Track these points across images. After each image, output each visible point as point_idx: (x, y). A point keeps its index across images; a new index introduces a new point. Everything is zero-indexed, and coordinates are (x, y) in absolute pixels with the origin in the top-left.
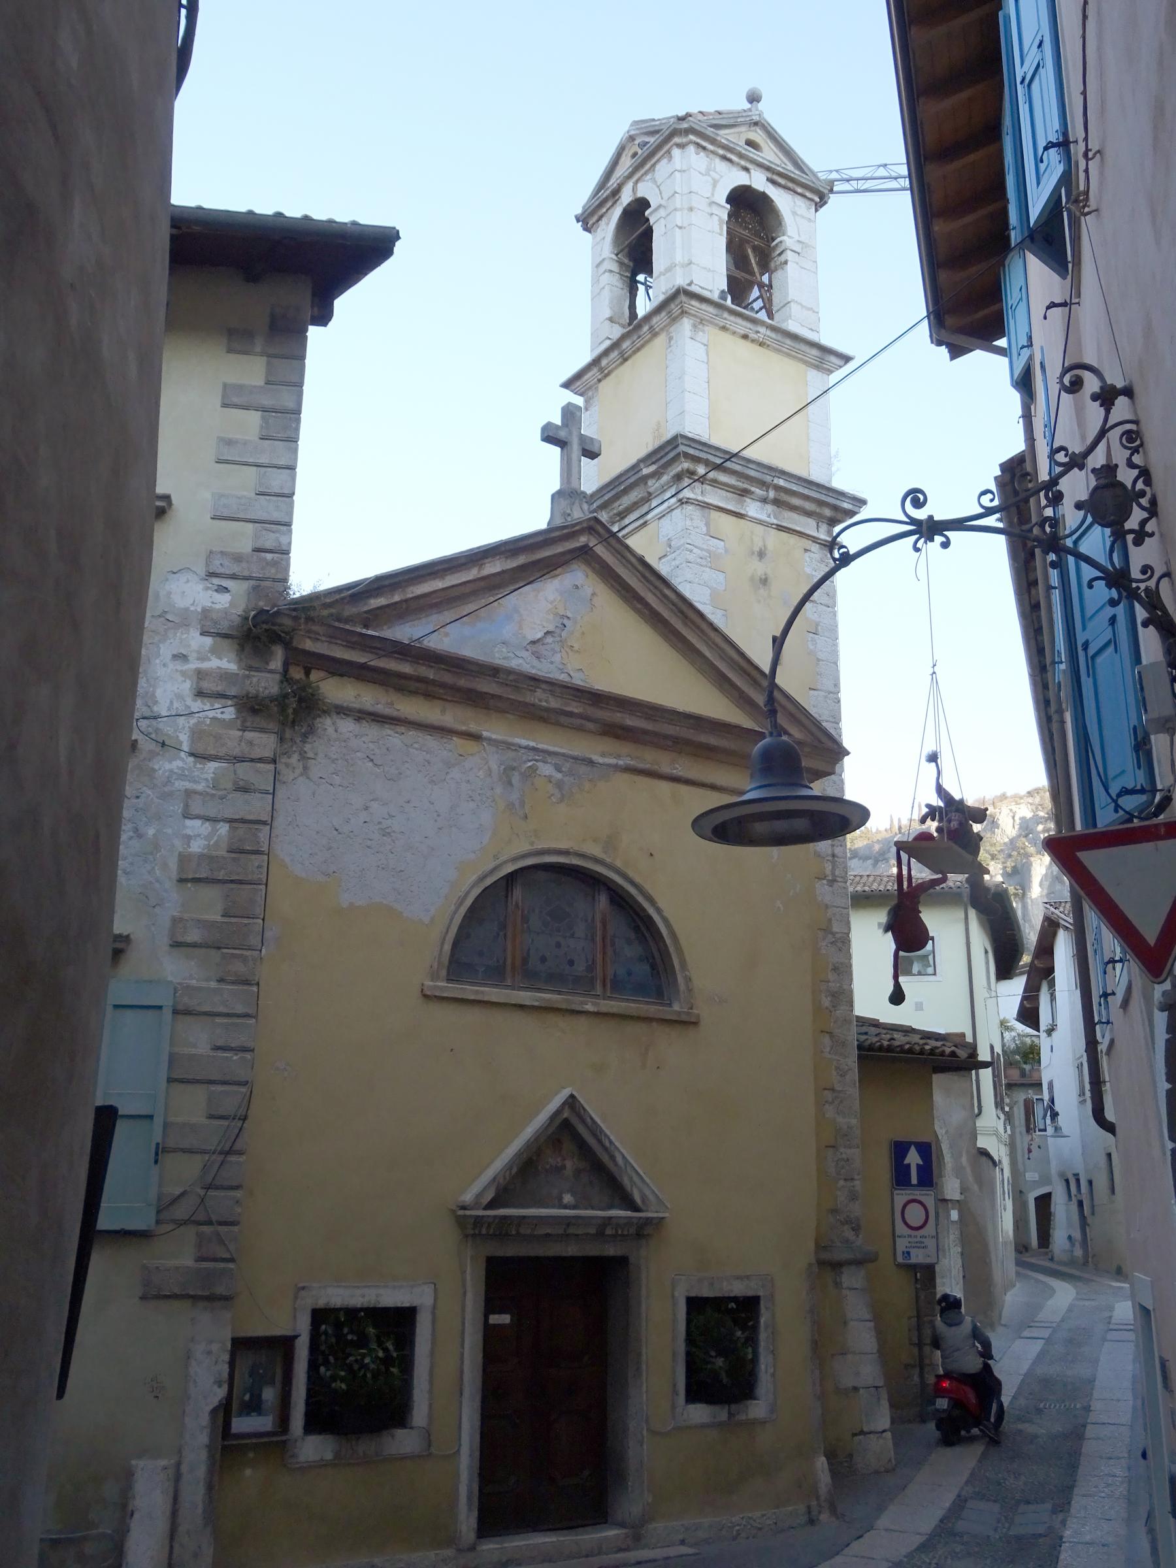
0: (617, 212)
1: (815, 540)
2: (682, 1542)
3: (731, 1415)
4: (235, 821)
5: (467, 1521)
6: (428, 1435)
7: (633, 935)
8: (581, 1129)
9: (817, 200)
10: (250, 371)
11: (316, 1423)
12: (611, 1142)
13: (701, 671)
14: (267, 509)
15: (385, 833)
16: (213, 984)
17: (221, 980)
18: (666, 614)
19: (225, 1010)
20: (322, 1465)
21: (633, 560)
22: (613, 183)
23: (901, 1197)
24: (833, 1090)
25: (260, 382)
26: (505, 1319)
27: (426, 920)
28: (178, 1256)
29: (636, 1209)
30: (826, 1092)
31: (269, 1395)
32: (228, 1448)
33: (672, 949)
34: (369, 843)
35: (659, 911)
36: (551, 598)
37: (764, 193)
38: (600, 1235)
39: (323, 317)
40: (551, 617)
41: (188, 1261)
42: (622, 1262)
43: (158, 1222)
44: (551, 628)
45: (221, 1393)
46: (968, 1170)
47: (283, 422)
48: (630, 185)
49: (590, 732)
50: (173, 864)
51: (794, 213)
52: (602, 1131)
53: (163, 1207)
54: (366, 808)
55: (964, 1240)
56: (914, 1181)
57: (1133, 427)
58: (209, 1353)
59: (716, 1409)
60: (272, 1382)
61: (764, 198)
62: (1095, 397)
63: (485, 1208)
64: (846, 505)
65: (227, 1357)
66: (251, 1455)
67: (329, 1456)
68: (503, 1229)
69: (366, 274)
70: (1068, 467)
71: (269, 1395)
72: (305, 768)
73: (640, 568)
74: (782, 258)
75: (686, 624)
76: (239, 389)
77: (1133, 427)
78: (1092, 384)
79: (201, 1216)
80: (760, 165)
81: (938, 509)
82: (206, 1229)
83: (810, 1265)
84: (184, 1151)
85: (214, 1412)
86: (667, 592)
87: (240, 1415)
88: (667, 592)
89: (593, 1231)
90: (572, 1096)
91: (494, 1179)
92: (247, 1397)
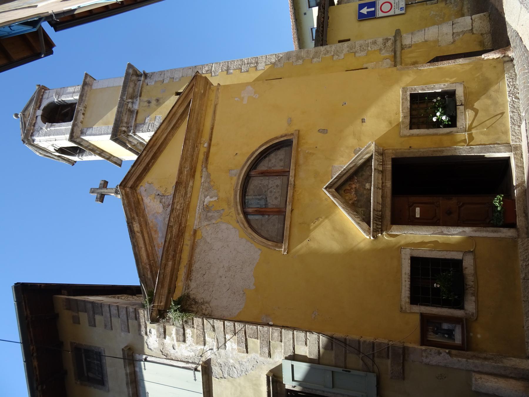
1: (144, 81)
2: (519, 126)
3: (462, 105)
4: (224, 332)
5: (506, 233)
7: (267, 159)
11: (459, 304)
12: (344, 170)
13: (173, 136)
15: (229, 269)
16: (283, 344)
17: (281, 341)
18: (152, 154)
20: (477, 302)
21: (133, 169)
23: (379, 14)
24: (333, 56)
27: (260, 252)
28: (387, 365)
29: (372, 155)
30: (334, 59)
31: (445, 326)
32: (467, 346)
33: (271, 144)
34: (232, 277)
35: (257, 150)
36: (149, 200)
37: (43, 110)
38: (382, 172)
40: (155, 200)
41: (389, 362)
43: (374, 372)
44: (159, 200)
50: (243, 355)
51: (48, 98)
52: (340, 174)
53: (368, 370)
54: (221, 277)
56: (373, 9)
58: (427, 357)
64: (131, 71)
66: (471, 334)
67: (473, 298)
68: (380, 218)
71: (445, 326)
72: (207, 303)
73: (135, 167)
75: (156, 145)
76: (90, 322)
79: (371, 357)
80: (35, 113)
82: (376, 355)
84: (345, 360)
87: (454, 340)
90: (326, 188)
92: (446, 336)
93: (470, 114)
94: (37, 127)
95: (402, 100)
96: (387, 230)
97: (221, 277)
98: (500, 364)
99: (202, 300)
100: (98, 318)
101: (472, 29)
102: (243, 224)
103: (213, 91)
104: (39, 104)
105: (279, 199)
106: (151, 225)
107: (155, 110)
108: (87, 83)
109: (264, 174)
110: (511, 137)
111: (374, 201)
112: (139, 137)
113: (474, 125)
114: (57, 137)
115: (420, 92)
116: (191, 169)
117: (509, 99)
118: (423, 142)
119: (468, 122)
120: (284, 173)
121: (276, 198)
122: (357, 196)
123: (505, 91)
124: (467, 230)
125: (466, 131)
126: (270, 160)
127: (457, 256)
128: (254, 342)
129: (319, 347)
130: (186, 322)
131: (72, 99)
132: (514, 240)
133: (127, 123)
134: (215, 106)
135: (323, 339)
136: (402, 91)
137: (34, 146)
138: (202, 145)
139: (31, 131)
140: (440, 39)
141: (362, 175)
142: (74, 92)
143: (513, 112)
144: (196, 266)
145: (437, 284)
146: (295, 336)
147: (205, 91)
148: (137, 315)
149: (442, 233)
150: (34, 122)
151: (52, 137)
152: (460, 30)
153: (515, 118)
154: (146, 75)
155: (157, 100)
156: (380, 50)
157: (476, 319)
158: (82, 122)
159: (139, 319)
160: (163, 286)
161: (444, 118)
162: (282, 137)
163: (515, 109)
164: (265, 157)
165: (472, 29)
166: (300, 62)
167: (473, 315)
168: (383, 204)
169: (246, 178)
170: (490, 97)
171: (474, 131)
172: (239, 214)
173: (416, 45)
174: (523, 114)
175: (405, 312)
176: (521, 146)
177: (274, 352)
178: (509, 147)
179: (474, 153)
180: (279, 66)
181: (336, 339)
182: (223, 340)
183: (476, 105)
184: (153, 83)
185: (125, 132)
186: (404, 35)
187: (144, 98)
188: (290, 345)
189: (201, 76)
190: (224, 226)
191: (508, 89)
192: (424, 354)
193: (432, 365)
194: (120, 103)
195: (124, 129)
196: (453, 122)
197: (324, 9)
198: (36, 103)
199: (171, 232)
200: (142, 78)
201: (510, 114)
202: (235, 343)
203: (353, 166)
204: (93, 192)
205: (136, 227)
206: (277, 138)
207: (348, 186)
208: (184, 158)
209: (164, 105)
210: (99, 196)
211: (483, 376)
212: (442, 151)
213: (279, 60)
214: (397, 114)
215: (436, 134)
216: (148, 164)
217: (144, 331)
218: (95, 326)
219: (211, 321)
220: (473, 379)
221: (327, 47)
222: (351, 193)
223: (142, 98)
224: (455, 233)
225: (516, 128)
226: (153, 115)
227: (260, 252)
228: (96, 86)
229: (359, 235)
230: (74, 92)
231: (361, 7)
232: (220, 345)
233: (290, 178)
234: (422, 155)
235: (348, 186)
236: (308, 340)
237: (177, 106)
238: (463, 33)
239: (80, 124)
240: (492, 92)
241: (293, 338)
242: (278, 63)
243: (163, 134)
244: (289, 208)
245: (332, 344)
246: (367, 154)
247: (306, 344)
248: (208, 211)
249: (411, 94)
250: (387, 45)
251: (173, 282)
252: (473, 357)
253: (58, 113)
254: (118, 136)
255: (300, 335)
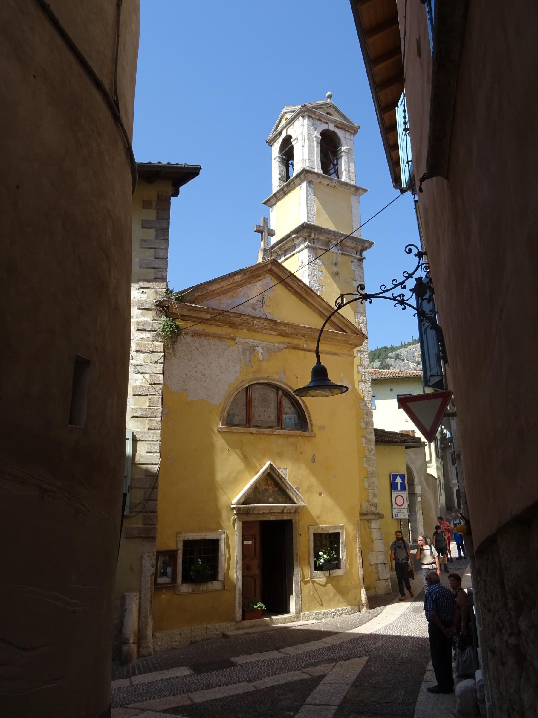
0: (280, 140)
1: (355, 258)
2: (314, 619)
3: (330, 574)
4: (152, 373)
5: (239, 613)
6: (223, 583)
7: (291, 406)
8: (274, 475)
9: (353, 132)
10: (151, 215)
11: (186, 579)
12: (285, 480)
13: (314, 311)
14: (158, 264)
15: (203, 375)
16: (146, 430)
17: (148, 429)
18: (300, 291)
19: (150, 439)
20: (188, 593)
22: (279, 129)
24: (366, 457)
25: (154, 218)
26: (250, 542)
27: (218, 404)
29: (294, 503)
31: (169, 570)
32: (157, 587)
36: (259, 288)
38: (282, 512)
39: (176, 194)
41: (140, 525)
42: (290, 522)
43: (130, 512)
45: (153, 570)
46: (424, 482)
47: (163, 232)
48: (285, 130)
49: (274, 335)
51: (345, 138)
52: (282, 476)
54: (196, 367)
55: (423, 508)
56: (399, 488)
57: (427, 265)
58: (148, 556)
59: (325, 572)
60: (170, 566)
61: (334, 132)
62: (416, 255)
63: (242, 504)
64: (367, 245)
65: (155, 558)
66: (164, 590)
68: (248, 512)
69: (190, 180)
70: (408, 278)
71: (169, 570)
72: (175, 354)
74: (341, 155)
75: (307, 295)
77: (427, 265)
78: (415, 251)
81: (368, 291)
82: (146, 514)
83: (358, 521)
85: (152, 575)
86: (300, 284)
87: (160, 577)
88: (300, 284)
89: (279, 511)
90: (271, 464)
91: (244, 494)
92: (162, 571)
93: (323, 580)
94: (318, 123)
95: (336, 526)
96: (239, 518)
97: (196, 367)
98: (148, 613)
99: (176, 349)
100: (152, 232)
101: (380, 580)
102: (240, 387)
103: (350, 351)
104: (340, 126)
105: (259, 419)
106: (238, 291)
107: (328, 271)
108: (357, 190)
109: (279, 404)
110: (306, 613)
111: (261, 507)
112: (302, 250)
113: (315, 584)
114: (306, 148)
115: (340, 541)
116: (286, 333)
117: (333, 610)
118: (304, 544)
119: (317, 580)
120: (280, 424)
121: (260, 416)
122: (263, 491)
123: (339, 607)
124: (240, 584)
125: (311, 578)
126: (290, 408)
127: (221, 577)
128: (145, 402)
129: (147, 464)
130: (158, 335)
131: (343, 169)
132: (233, 619)
133: (318, 239)
134: (337, 354)
135: (155, 468)
136: (342, 526)
137: (298, 115)
138: (305, 342)
139: (313, 116)
140: (374, 553)
141: (279, 494)
142: (349, 172)
143: (324, 613)
144: (204, 341)
145: (201, 561)
146: (156, 442)
147: (350, 344)
148: (160, 280)
149: (237, 563)
150: (323, 120)
151: (306, 141)
152: (380, 569)
153: (320, 615)
154: (361, 260)
155: (337, 274)
156: (368, 501)
157: (175, 594)
158: (320, 182)
159: (157, 281)
160: (189, 310)
161: (322, 561)
162: (311, 421)
163: (326, 615)
164: (293, 404)
165: (380, 580)
166: (363, 426)
167: (179, 591)
168: (258, 514)
169: (276, 386)
170: (335, 596)
171: (311, 584)
172: (248, 382)
173: (370, 533)
174: (323, 621)
175: (177, 537)
176: (299, 620)
177: (136, 421)
178: (299, 612)
179: (295, 586)
180: (361, 405)
181: (157, 480)
182: (144, 372)
183: (329, 586)
184: (353, 269)
185: (310, 236)
186: (379, 522)
187: (340, 259)
188: (146, 437)
189: (363, 341)
190: (238, 368)
191: (340, 609)
192: (151, 554)
193: (141, 561)
194: (338, 233)
195: (313, 236)
196: (318, 568)
197: (404, 442)
198: (342, 124)
199: (235, 317)
200: (358, 257)
201: (322, 611)
202: (142, 383)
203: (287, 488)
204: (264, 221)
205: (238, 278)
206: (309, 416)
207: (273, 484)
208: (296, 327)
209: (332, 281)
210: (261, 229)
211: (138, 601)
212: (297, 560)
213: (366, 404)
214: (325, 523)
215: (309, 555)
216: (291, 287)
217: (143, 286)
218: (143, 227)
219: (162, 361)
220: (135, 594)
221: (373, 446)
222: (265, 485)
223: (340, 256)
224: (238, 574)
225: (313, 617)
226: (323, 269)
227: (218, 404)
228: (354, 198)
229: (236, 496)
230: (349, 172)
231: (402, 477)
232: (138, 367)
233: (278, 431)
234: (294, 545)
235: (273, 484)
236: (152, 454)
237: (340, 317)
238: (378, 573)
239: (318, 180)
240: (339, 597)
241: (153, 441)
242: (363, 404)
243: (316, 302)
244: (254, 430)
245: (152, 476)
246: (297, 499)
247: (149, 452)
248: (250, 351)
249: (338, 533)
250: (372, 506)
251: (191, 319)
252: (151, 592)
253: (329, 147)
254: (306, 231)
255: (157, 447)
